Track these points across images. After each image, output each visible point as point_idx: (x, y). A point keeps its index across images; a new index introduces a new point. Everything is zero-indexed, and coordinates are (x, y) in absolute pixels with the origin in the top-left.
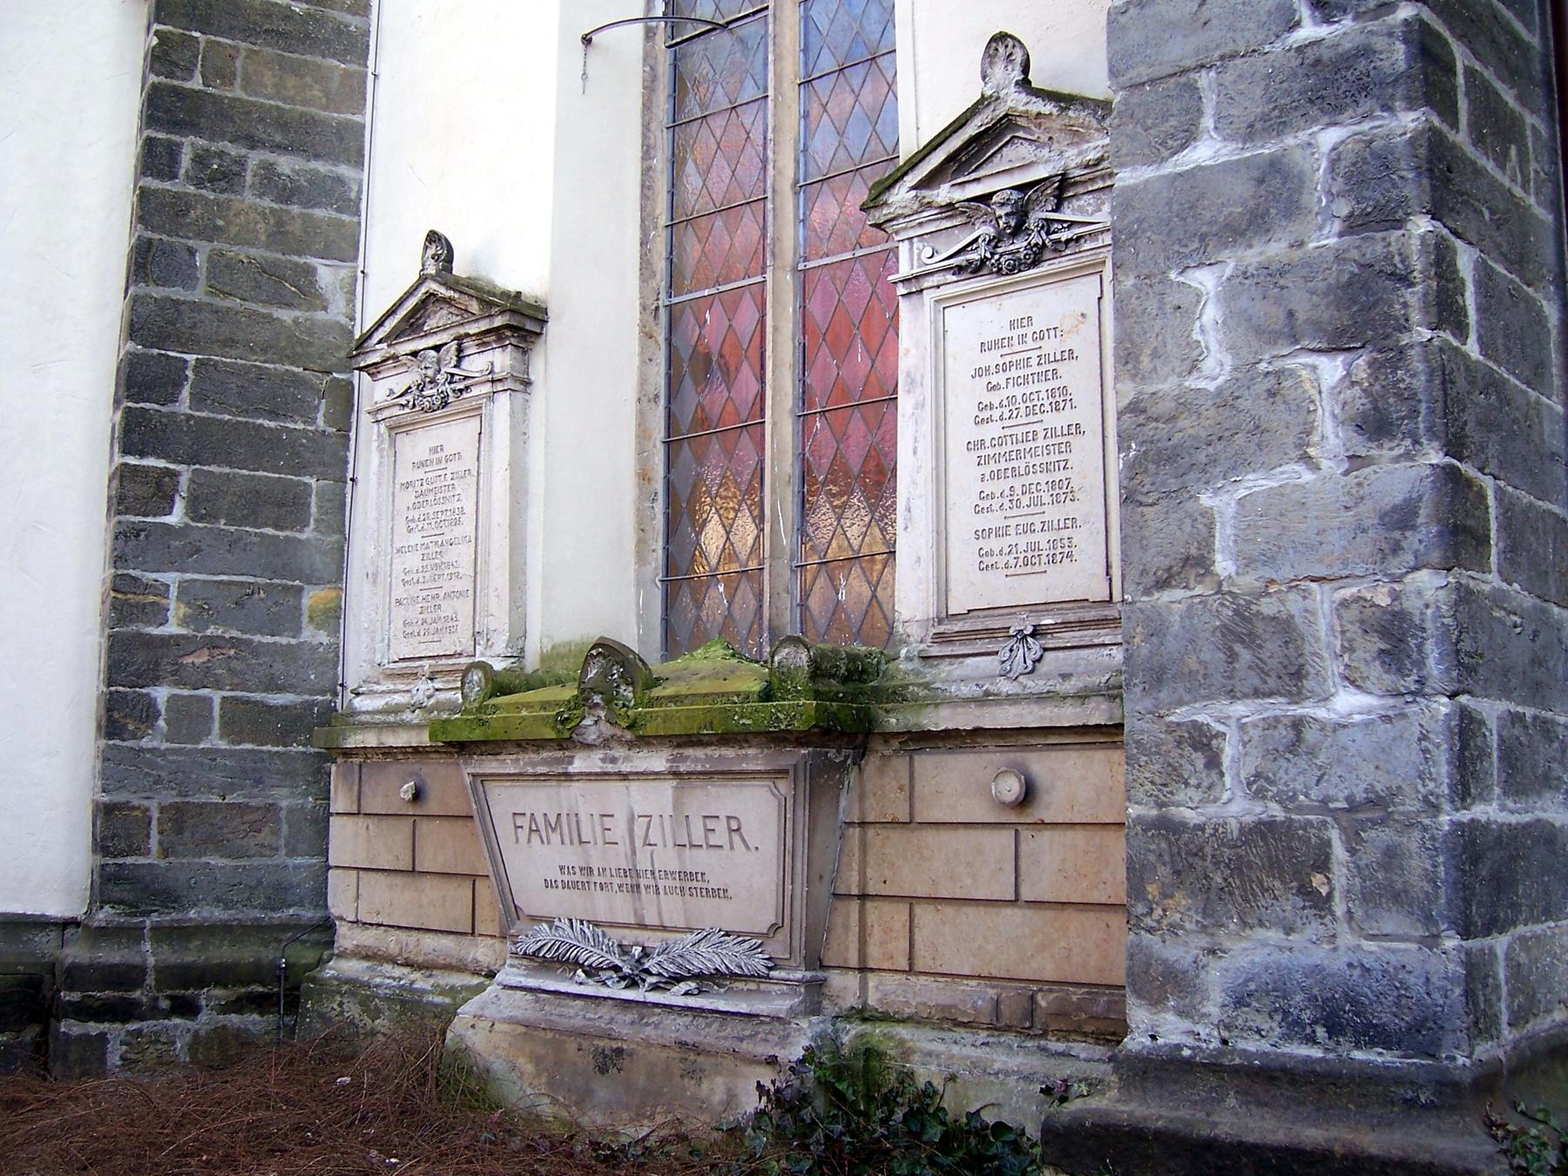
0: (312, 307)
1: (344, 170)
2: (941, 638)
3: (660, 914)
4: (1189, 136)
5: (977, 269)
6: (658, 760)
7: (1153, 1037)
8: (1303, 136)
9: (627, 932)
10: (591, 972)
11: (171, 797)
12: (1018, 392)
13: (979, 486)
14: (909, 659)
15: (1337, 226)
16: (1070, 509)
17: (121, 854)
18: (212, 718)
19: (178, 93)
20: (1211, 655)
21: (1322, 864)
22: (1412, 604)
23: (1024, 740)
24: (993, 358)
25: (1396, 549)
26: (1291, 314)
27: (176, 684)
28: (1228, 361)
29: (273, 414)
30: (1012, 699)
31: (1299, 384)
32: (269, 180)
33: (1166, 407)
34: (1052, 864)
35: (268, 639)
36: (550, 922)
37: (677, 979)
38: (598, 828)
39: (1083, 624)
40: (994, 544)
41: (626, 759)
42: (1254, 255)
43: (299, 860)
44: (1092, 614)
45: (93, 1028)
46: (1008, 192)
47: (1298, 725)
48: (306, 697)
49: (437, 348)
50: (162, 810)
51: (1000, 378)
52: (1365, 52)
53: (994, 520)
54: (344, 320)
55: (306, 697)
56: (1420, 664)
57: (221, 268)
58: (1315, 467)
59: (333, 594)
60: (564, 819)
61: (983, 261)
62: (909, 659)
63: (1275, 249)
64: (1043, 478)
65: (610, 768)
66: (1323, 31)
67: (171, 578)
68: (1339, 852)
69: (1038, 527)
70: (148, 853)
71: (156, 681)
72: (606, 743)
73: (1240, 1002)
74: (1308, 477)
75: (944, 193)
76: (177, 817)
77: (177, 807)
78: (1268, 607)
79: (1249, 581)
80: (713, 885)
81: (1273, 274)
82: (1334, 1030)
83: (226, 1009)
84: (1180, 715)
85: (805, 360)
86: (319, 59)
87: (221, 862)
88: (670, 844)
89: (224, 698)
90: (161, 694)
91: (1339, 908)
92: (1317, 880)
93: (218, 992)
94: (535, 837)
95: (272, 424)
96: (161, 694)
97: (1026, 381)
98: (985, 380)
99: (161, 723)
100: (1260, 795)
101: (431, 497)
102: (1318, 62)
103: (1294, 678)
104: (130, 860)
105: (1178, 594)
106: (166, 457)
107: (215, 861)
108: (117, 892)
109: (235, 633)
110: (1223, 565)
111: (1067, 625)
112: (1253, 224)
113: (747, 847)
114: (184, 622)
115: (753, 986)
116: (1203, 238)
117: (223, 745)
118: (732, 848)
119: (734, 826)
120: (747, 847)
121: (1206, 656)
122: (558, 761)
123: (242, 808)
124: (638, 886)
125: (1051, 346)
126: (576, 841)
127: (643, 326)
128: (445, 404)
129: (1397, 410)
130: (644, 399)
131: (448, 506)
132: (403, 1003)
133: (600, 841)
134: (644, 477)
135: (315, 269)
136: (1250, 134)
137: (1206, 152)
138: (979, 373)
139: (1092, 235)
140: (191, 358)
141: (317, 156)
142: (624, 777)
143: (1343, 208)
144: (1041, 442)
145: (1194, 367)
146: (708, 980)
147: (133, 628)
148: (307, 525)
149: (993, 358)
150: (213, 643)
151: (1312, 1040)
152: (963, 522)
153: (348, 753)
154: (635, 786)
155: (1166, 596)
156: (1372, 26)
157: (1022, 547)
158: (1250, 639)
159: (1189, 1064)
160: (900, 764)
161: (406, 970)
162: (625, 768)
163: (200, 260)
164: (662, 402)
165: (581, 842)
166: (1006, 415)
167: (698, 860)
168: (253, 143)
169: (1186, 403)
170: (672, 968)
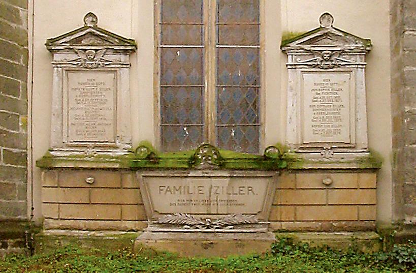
0: (19, 24)
3: (217, 210)
7: (410, 221)
10: (191, 226)
14: (291, 152)
23: (338, 171)
41: (212, 173)
43: (20, 201)
49: (96, 50)
51: (320, 92)
54: (26, 29)
69: (331, 126)
75: (307, 47)
83: (13, 246)
85: (219, 71)
87: (4, 201)
93: (12, 241)
95: (11, 61)
98: (316, 92)
101: (89, 94)
109: (5, 129)
113: (254, 194)
115: (250, 226)
120: (254, 194)
126: (186, 193)
130: (156, 73)
134: (155, 96)
135: (18, 11)
144: (332, 108)
154: (213, 179)
160: (292, 175)
166: (322, 100)
170: (225, 223)
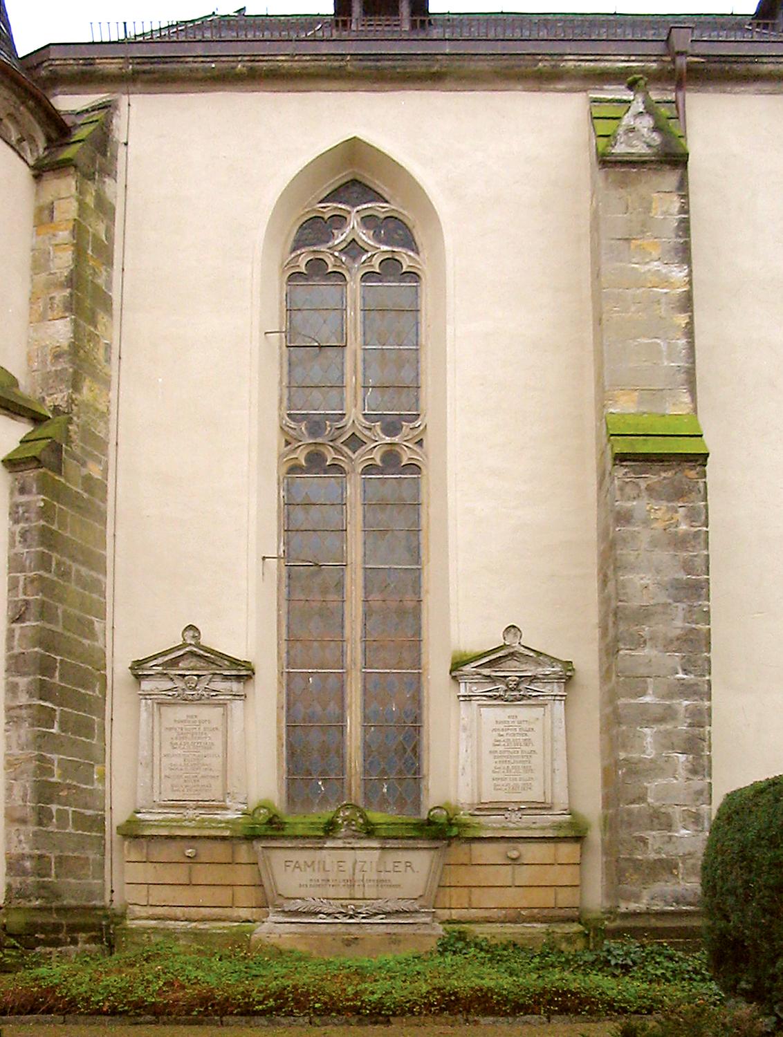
1: (101, 577)
2: (479, 809)
4: (644, 694)
5: (496, 698)
6: (375, 844)
8: (678, 701)
9: (342, 901)
11: (57, 853)
12: (511, 738)
13: (494, 765)
15: (686, 725)
16: (530, 775)
17: (44, 877)
18: (68, 819)
19: (50, 530)
20: (647, 821)
21: (676, 867)
22: (701, 812)
24: (502, 726)
25: (698, 800)
26: (673, 743)
27: (59, 804)
28: (654, 752)
29: (83, 686)
30: (512, 829)
31: (674, 760)
32: (79, 577)
33: (635, 761)
34: (524, 875)
35: (85, 786)
36: (302, 899)
37: (376, 914)
38: (336, 866)
39: (536, 808)
40: (500, 782)
41: (356, 843)
42: (662, 727)
43: (96, 881)
44: (539, 806)
45: (49, 949)
46: (504, 672)
47: (670, 837)
48: (96, 812)
49: (198, 676)
50: (56, 858)
52: (696, 684)
53: (501, 776)
54: (103, 647)
55: (96, 812)
56: (703, 825)
57: (67, 616)
58: (677, 779)
59: (102, 768)
60: (316, 863)
61: (500, 696)
62: (464, 815)
63: (669, 727)
64: (520, 765)
65: (348, 846)
66: (685, 676)
67: (55, 757)
68: (680, 865)
70: (49, 876)
71: (52, 802)
72: (347, 837)
73: (653, 899)
74: (675, 781)
75: (486, 672)
76: (61, 860)
77: (60, 857)
78: (663, 810)
79: (657, 804)
80: (394, 883)
81: (667, 734)
82: (678, 903)
83: (86, 942)
84: (637, 834)
86: (92, 522)
88: (374, 870)
89: (74, 811)
90: (54, 807)
91: (680, 876)
92: (675, 872)
94: (298, 870)
95: (83, 691)
96: (54, 807)
97: (514, 735)
99: (54, 820)
100: (659, 853)
101: (189, 736)
102: (683, 684)
103: (669, 827)
104: (46, 879)
105: (637, 806)
106: (51, 702)
107: (72, 881)
108: (43, 892)
109: (75, 783)
110: (650, 800)
111: (529, 808)
112: (661, 720)
114: (59, 777)
116: (648, 721)
117: (73, 831)
118: (406, 871)
119: (408, 864)
120: (413, 871)
121: (646, 821)
122: (319, 843)
123: (78, 858)
124: (354, 886)
125: (524, 726)
126: (322, 869)
127: (279, 680)
128: (200, 699)
129: (700, 769)
130: (280, 708)
131: (204, 741)
132: (196, 934)
133: (335, 869)
134: (279, 738)
136: (663, 697)
137: (647, 699)
138: (494, 730)
139: (543, 696)
140: (58, 658)
141: (93, 569)
142: (353, 848)
143: (689, 721)
145: (644, 752)
146: (388, 914)
147: (44, 778)
148: (94, 737)
149: (502, 726)
150: (69, 787)
151: (672, 906)
152: (487, 775)
153: (143, 836)
155: (633, 806)
156: (699, 678)
157: (512, 784)
158: (658, 818)
159: (639, 914)
160: (466, 846)
161: (186, 923)
162: (356, 846)
163: (59, 612)
164: (285, 709)
165: (324, 869)
167: (383, 876)
168: (75, 560)
169: (641, 761)
170: (374, 911)
